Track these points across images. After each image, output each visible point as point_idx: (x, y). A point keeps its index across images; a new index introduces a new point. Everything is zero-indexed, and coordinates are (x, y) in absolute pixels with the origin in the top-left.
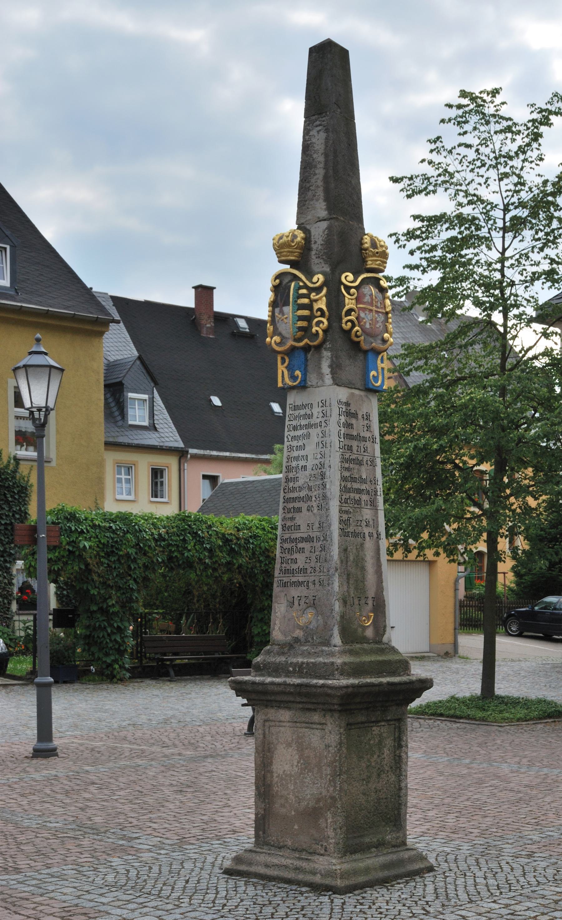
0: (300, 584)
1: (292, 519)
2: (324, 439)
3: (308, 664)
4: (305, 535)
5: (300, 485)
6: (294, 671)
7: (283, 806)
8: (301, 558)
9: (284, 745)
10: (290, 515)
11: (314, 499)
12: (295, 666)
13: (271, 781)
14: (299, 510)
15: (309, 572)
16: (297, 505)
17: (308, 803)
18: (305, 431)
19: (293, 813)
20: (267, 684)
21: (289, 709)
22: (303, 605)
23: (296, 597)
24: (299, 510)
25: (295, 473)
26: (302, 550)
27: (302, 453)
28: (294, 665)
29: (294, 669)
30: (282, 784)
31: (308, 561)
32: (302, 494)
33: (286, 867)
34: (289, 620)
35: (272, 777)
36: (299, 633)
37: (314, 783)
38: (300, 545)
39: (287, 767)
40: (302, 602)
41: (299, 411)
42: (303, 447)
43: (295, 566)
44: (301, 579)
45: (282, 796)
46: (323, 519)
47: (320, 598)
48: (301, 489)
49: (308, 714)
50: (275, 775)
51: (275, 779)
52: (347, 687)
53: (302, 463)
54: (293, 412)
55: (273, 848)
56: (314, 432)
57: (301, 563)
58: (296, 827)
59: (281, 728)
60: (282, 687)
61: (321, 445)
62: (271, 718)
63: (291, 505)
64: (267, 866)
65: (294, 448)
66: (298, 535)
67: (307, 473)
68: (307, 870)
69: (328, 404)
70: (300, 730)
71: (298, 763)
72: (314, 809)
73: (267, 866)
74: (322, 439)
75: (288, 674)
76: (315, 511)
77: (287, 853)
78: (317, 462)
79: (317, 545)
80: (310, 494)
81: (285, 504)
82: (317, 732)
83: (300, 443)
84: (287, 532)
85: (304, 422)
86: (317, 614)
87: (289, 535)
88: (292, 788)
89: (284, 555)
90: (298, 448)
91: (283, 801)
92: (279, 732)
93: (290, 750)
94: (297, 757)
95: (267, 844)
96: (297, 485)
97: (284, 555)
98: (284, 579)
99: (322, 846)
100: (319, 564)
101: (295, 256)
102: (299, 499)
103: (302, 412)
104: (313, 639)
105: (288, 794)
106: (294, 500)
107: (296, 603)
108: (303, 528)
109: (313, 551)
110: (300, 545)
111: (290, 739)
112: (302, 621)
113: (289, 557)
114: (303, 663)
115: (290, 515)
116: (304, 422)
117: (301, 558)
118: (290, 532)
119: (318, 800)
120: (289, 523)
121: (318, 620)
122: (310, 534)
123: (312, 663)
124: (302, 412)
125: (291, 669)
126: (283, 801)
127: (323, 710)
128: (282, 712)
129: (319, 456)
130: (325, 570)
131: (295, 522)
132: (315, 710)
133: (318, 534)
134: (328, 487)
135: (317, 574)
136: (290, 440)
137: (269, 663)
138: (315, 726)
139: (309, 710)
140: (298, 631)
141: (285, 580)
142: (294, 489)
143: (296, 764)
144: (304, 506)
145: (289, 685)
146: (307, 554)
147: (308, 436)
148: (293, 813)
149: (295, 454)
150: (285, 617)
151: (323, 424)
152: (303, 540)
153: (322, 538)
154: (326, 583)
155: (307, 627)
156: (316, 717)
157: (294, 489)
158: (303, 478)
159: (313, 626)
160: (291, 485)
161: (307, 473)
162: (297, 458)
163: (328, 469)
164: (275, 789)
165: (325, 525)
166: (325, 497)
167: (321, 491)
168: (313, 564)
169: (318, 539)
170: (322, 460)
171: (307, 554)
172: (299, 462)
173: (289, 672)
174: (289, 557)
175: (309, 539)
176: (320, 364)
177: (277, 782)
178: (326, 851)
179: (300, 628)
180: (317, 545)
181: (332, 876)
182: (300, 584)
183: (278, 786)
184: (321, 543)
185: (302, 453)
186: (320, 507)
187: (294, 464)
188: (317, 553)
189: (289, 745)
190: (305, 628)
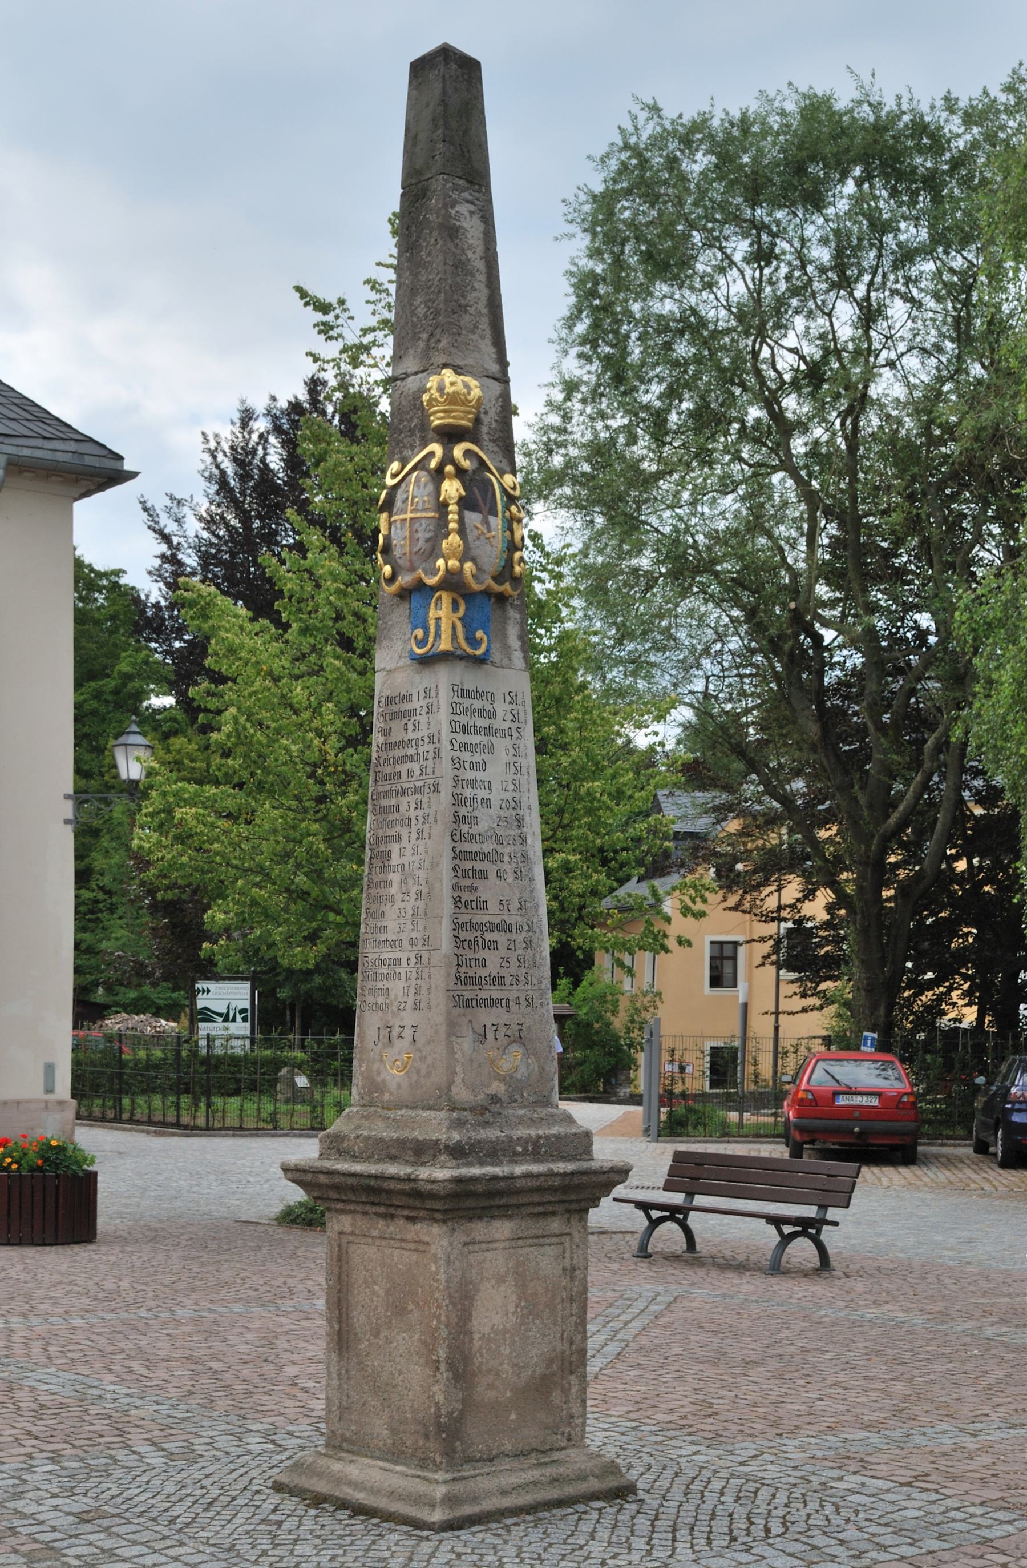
0: (493, 1003)
1: (471, 889)
2: (519, 759)
3: (547, 1138)
4: (496, 920)
5: (482, 831)
6: (525, 1152)
7: (490, 1386)
8: (493, 961)
9: (493, 1282)
10: (468, 882)
11: (506, 858)
12: (527, 1142)
13: (470, 1349)
14: (483, 875)
15: (507, 982)
16: (479, 865)
17: (534, 1371)
18: (485, 739)
19: (509, 1394)
20: (518, 1177)
21: (509, 1217)
22: (502, 1040)
23: (489, 1025)
24: (483, 875)
25: (470, 809)
26: (492, 945)
27: (480, 775)
28: (525, 1141)
29: (525, 1149)
30: (490, 1349)
31: (505, 964)
32: (487, 847)
33: (535, 1483)
34: (480, 1065)
35: (471, 1340)
36: (498, 1088)
37: (544, 1335)
38: (489, 936)
39: (497, 1319)
40: (500, 1035)
41: (471, 701)
42: (483, 766)
43: (483, 973)
44: (496, 995)
45: (489, 1371)
46: (526, 896)
47: (529, 1028)
48: (482, 838)
49: (541, 1222)
50: (476, 1336)
51: (477, 1344)
52: (565, 1174)
53: (482, 793)
54: (460, 700)
55: (479, 1464)
56: (501, 744)
57: (493, 968)
58: (513, 1417)
59: (486, 1254)
60: (542, 1179)
61: (513, 769)
62: (478, 1238)
63: (468, 865)
64: (504, 1493)
65: (467, 765)
66: (485, 919)
67: (493, 811)
68: (572, 1476)
69: (433, 694)
70: (521, 1251)
71: (517, 1307)
72: (544, 1377)
73: (504, 1493)
74: (515, 759)
75: (514, 1158)
76: (510, 880)
77: (507, 1464)
78: (509, 796)
79: (520, 938)
80: (500, 849)
81: (457, 861)
82: (551, 1251)
83: (477, 758)
84: (463, 910)
85: (481, 723)
86: (527, 1054)
87: (469, 917)
88: (507, 1351)
89: (461, 951)
90: (474, 766)
91: (490, 1378)
92: (484, 1261)
93: (503, 1288)
94: (514, 1297)
95: (469, 1460)
96: (474, 830)
97: (461, 951)
98: (465, 993)
99: (563, 1433)
100: (524, 971)
101: (469, 420)
102: (485, 856)
103: (477, 704)
104: (522, 1096)
105: (501, 1364)
106: (473, 856)
107: (490, 1035)
108: (493, 907)
109: (512, 947)
110: (489, 936)
111: (503, 1270)
112: (505, 1065)
113: (470, 955)
114: (539, 1137)
115: (468, 882)
116: (481, 723)
117: (493, 961)
118: (470, 911)
119: (551, 1362)
120: (466, 896)
121: (528, 1065)
122: (505, 917)
123: (554, 1136)
124: (477, 704)
125: (519, 1149)
126: (490, 1378)
127: (568, 1211)
128: (497, 1224)
129: (511, 787)
130: (535, 981)
131: (479, 894)
132: (553, 1213)
133: (519, 919)
134: (529, 841)
135: (521, 986)
136: (457, 747)
137: (479, 1142)
138: (547, 1241)
139: (544, 1214)
140: (496, 1083)
141: (467, 995)
142: (471, 838)
143: (512, 1310)
144: (492, 869)
145: (558, 1174)
146: (502, 952)
147: (490, 749)
148: (509, 1394)
149: (470, 775)
150: (471, 1060)
151: (515, 734)
152: (493, 927)
153: (526, 928)
154: (537, 1002)
155: (511, 1077)
156: (555, 1225)
157: (471, 838)
158: (485, 821)
159: (522, 1073)
160: (465, 828)
161: (493, 811)
162: (472, 784)
163: (527, 811)
164: (477, 1360)
165: (528, 905)
166: (525, 857)
167: (519, 848)
168: (513, 970)
169: (520, 929)
170: (517, 795)
171: (502, 952)
172: (476, 791)
173: (515, 1154)
174: (470, 955)
175: (504, 927)
176: (505, 629)
177: (480, 1348)
178: (569, 1440)
179: (502, 1079)
180: (520, 938)
181: (612, 1473)
182: (493, 1003)
183: (482, 1355)
184: (524, 934)
185: (480, 775)
186: (518, 875)
187: (468, 792)
188: (520, 952)
189: (501, 1280)
190: (507, 1079)
